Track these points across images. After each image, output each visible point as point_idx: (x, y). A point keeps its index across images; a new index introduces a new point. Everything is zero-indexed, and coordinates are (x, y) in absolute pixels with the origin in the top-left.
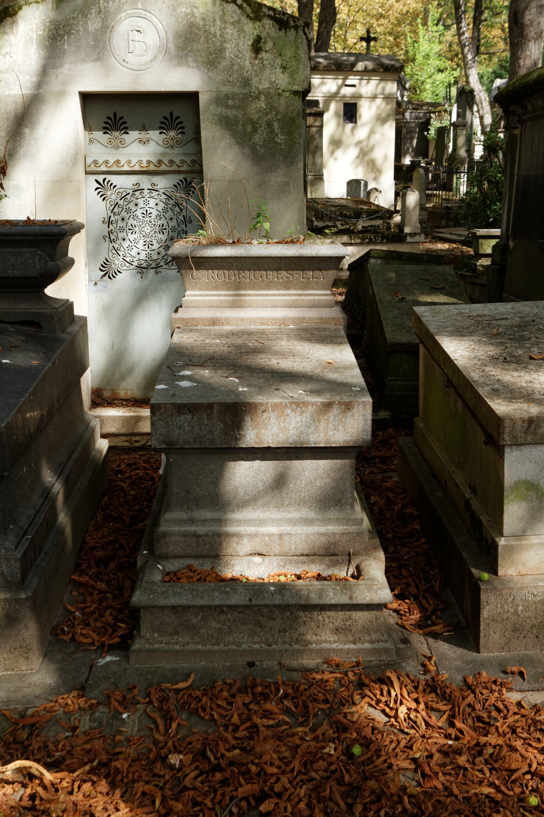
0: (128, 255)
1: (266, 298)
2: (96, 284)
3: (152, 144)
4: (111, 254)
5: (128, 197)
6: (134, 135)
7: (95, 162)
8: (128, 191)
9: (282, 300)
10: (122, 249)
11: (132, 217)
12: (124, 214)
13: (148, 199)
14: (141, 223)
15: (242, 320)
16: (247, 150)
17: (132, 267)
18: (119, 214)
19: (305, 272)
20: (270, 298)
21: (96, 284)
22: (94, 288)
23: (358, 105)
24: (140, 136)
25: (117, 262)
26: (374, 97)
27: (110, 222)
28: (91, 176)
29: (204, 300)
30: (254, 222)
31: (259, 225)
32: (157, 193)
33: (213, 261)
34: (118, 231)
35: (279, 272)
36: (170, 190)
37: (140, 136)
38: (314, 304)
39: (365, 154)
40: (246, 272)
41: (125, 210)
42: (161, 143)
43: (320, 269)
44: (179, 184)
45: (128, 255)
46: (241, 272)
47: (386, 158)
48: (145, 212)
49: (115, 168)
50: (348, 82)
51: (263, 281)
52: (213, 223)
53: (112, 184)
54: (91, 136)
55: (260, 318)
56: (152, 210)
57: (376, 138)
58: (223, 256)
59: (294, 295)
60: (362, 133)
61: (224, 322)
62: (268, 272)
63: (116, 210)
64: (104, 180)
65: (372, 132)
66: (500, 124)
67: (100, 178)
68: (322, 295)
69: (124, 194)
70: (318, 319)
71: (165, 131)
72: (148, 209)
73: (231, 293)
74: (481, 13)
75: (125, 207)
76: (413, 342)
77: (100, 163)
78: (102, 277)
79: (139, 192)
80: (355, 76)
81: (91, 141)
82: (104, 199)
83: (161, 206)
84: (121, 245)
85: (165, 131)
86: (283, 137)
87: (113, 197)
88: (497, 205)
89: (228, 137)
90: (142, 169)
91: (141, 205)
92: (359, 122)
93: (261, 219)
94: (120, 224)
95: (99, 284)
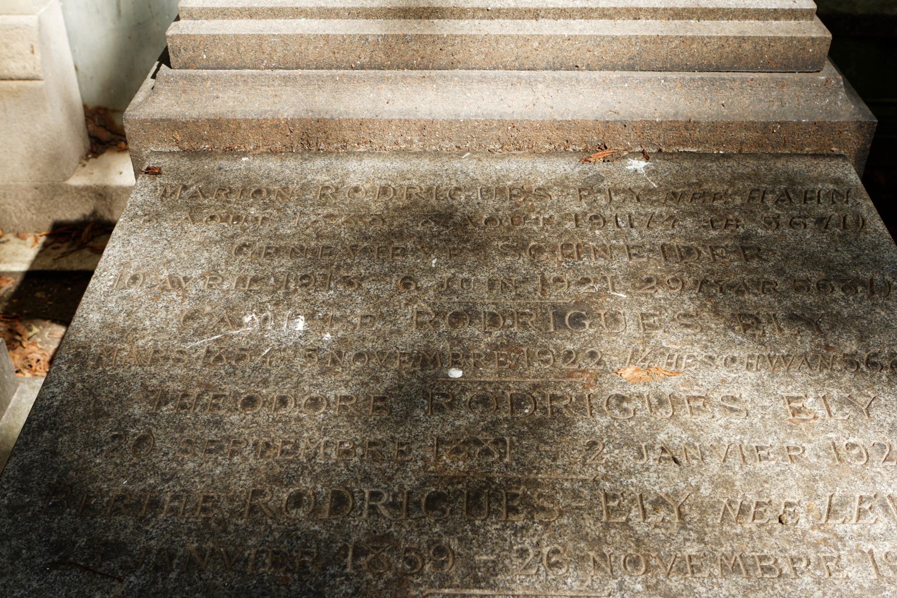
9: (599, 40)
38: (738, 58)
55: (502, 124)
61: (349, 135)
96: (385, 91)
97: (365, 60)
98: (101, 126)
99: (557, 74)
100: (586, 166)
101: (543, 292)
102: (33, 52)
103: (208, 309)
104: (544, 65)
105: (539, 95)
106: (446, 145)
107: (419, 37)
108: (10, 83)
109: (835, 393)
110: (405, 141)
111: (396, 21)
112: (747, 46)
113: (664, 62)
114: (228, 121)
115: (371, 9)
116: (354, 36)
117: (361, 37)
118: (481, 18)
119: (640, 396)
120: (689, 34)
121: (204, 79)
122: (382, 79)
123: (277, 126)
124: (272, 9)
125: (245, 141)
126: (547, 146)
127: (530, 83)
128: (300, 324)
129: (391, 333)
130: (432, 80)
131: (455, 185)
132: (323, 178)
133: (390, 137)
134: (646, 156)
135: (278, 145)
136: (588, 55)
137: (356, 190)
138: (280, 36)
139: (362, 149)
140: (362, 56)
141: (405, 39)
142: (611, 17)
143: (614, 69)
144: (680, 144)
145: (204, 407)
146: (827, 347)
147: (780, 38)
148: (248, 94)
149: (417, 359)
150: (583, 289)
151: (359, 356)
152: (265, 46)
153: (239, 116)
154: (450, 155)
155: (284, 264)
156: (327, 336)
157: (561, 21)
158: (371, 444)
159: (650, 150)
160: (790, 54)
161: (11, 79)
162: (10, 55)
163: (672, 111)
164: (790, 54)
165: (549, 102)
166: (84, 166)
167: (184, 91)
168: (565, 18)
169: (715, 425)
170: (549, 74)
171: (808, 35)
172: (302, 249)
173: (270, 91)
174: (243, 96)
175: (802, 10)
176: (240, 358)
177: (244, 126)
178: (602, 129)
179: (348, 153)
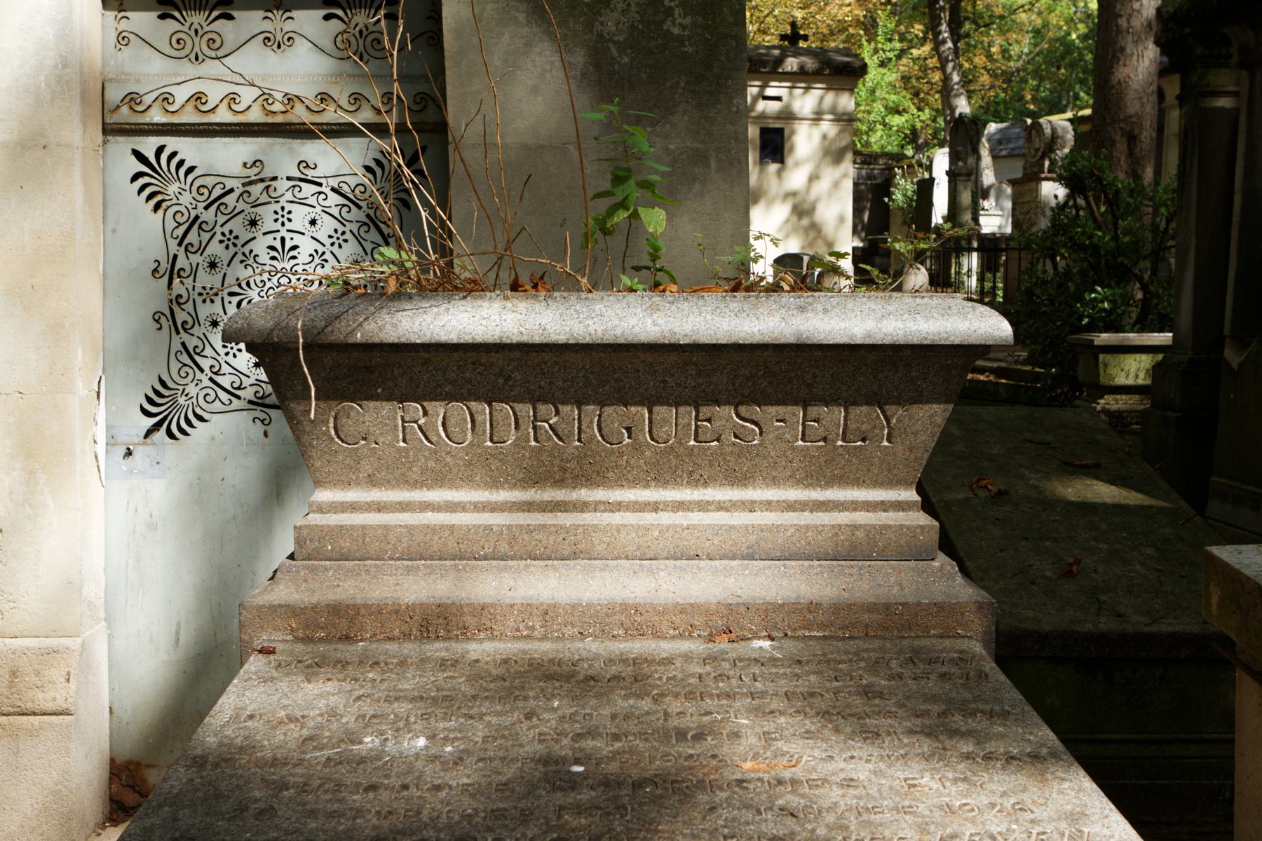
0: (225, 369)
1: (649, 518)
2: (129, 453)
3: (302, 47)
4: (175, 366)
5: (230, 200)
6: (251, 21)
7: (132, 99)
8: (230, 184)
9: (717, 529)
10: (208, 351)
11: (240, 257)
12: (215, 249)
13: (288, 207)
14: (265, 276)
15: (547, 612)
16: (579, 58)
17: (236, 403)
18: (201, 250)
19: (814, 411)
20: (666, 518)
21: (129, 453)
22: (125, 465)
23: (786, 133)
24: (267, 25)
25: (192, 390)
26: (817, 117)
27: (173, 273)
28: (121, 139)
29: (386, 528)
30: (603, 205)
31: (622, 215)
32: (316, 189)
33: (426, 362)
34: (199, 300)
35: (705, 411)
36: (353, 181)
37: (267, 25)
38: (853, 546)
39: (802, 211)
40: (565, 409)
41: (219, 237)
42: (327, 44)
43: (878, 400)
44: (378, 162)
45: (225, 369)
46: (543, 409)
47: (841, 219)
48: (278, 245)
49: (189, 117)
50: (770, 92)
51: (637, 448)
52: (433, 213)
53: (181, 163)
54: (124, 25)
55: (625, 607)
56: (298, 240)
57: (823, 185)
58: (467, 339)
59: (768, 505)
60: (796, 178)
61: (470, 621)
62: (660, 410)
63: (192, 237)
64: (160, 150)
65: (813, 178)
66: (1043, 165)
67: (148, 146)
68: (883, 506)
69: (217, 192)
70: (871, 608)
71: (340, 12)
72: (288, 236)
73: (503, 495)
74: (960, 25)
75: (218, 230)
76: (1077, 628)
77: (148, 99)
78: (149, 433)
79: (261, 186)
80: (780, 81)
81: (122, 39)
82: (157, 207)
83: (327, 225)
84: (205, 339)
85: (340, 12)
86: (688, 21)
87: (186, 199)
88: (1096, 292)
89: (521, 17)
90: (270, 120)
91: (268, 224)
92: (790, 161)
93: (631, 189)
94: (206, 279)
95: (139, 452)
96: (508, 580)
97: (488, 550)
98: (128, 786)
99: (678, 563)
100: (711, 645)
101: (666, 720)
102: (68, 680)
103: (327, 734)
104: (665, 554)
105: (661, 582)
106: (569, 631)
107: (543, 527)
108: (32, 718)
109: (950, 775)
110: (527, 628)
111: (520, 514)
112: (860, 534)
113: (782, 551)
114: (348, 606)
115: (496, 503)
116: (479, 526)
117: (486, 527)
118: (603, 511)
119: (760, 779)
120: (803, 523)
121: (326, 569)
122: (506, 569)
123: (397, 612)
124: (400, 503)
125: (362, 629)
126: (671, 632)
127: (651, 572)
128: (422, 742)
129: (513, 746)
130: (555, 569)
131: (577, 657)
132: (444, 654)
133: (511, 623)
134: (771, 638)
135: (396, 632)
136: (707, 544)
137: (477, 661)
138: (406, 527)
139: (482, 635)
140: (486, 546)
141: (529, 529)
142: (727, 510)
143: (733, 558)
144: (804, 628)
145: (326, 791)
146: (944, 749)
147: (890, 526)
148: (369, 583)
149: (539, 760)
150: (705, 719)
151: (480, 760)
152: (391, 536)
153: (359, 601)
154: (572, 638)
155: (403, 708)
156: (449, 749)
157: (680, 513)
158: (493, 811)
159: (775, 634)
160: (903, 542)
161: (35, 714)
162: (39, 684)
163: (794, 595)
164: (903, 542)
165: (671, 588)
166: (99, 835)
167: (305, 581)
168: (684, 510)
169: (833, 794)
170: (671, 563)
171: (915, 523)
172: (422, 698)
173: (392, 580)
174: (364, 585)
175: (907, 502)
176: (359, 763)
177: (363, 611)
178: (725, 612)
179: (468, 639)
